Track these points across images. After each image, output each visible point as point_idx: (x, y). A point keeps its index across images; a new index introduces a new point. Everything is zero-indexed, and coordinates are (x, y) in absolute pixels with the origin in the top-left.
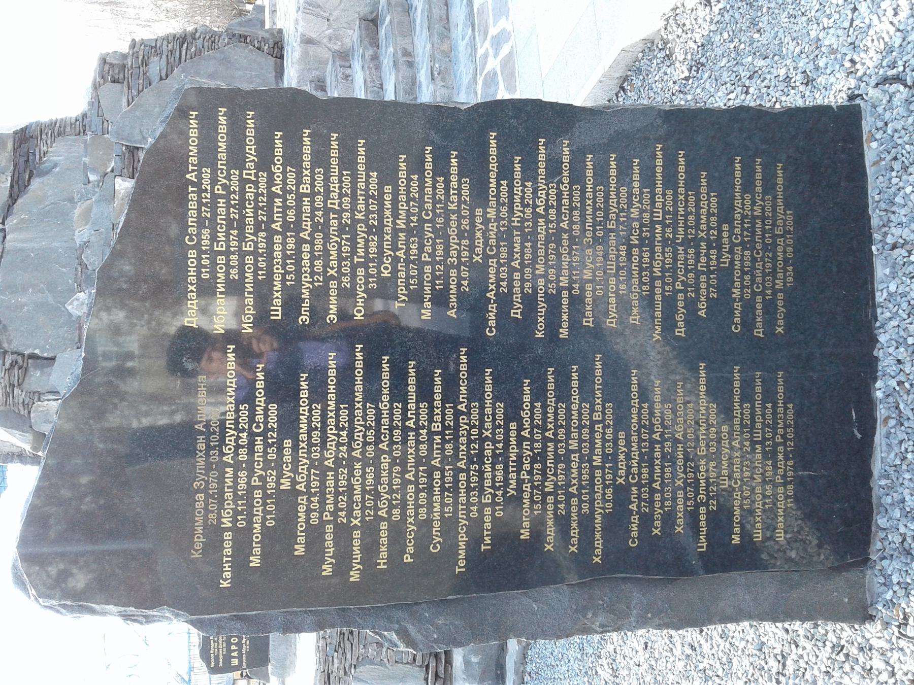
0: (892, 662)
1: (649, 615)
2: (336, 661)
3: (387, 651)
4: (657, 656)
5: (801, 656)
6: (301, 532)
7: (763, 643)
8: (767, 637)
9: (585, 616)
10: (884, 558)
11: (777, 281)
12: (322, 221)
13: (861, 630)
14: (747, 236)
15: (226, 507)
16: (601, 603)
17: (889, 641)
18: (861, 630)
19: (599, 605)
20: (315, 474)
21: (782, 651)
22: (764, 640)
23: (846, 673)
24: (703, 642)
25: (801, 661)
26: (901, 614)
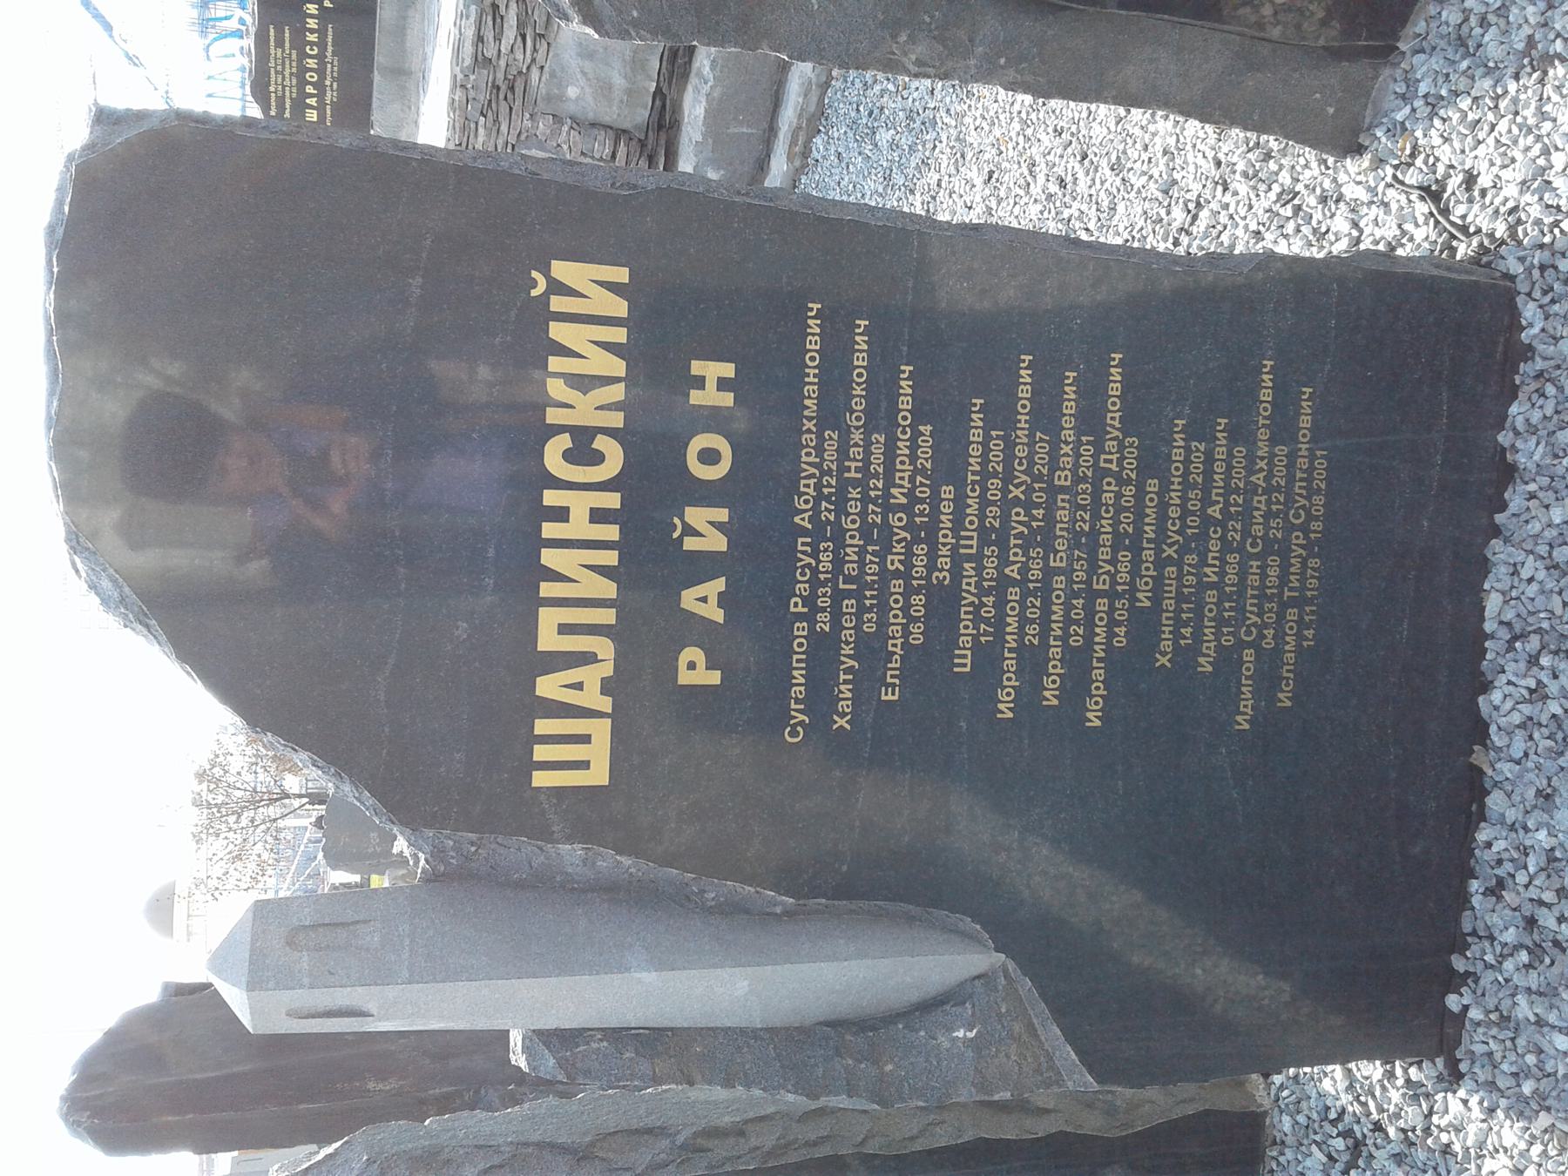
0: (1362, 224)
1: (1002, 61)
2: (481, 131)
3: (569, 133)
4: (1002, 194)
5: (1226, 207)
7: (1175, 182)
8: (1184, 173)
9: (894, 37)
10: (1422, 51)
12: (1130, 530)
13: (1335, 168)
14: (986, 633)
16: (928, 20)
17: (1372, 190)
18: (1335, 168)
19: (924, 22)
21: (1199, 196)
22: (1177, 176)
23: (1286, 236)
24: (1081, 175)
25: (1223, 213)
26: (1408, 146)
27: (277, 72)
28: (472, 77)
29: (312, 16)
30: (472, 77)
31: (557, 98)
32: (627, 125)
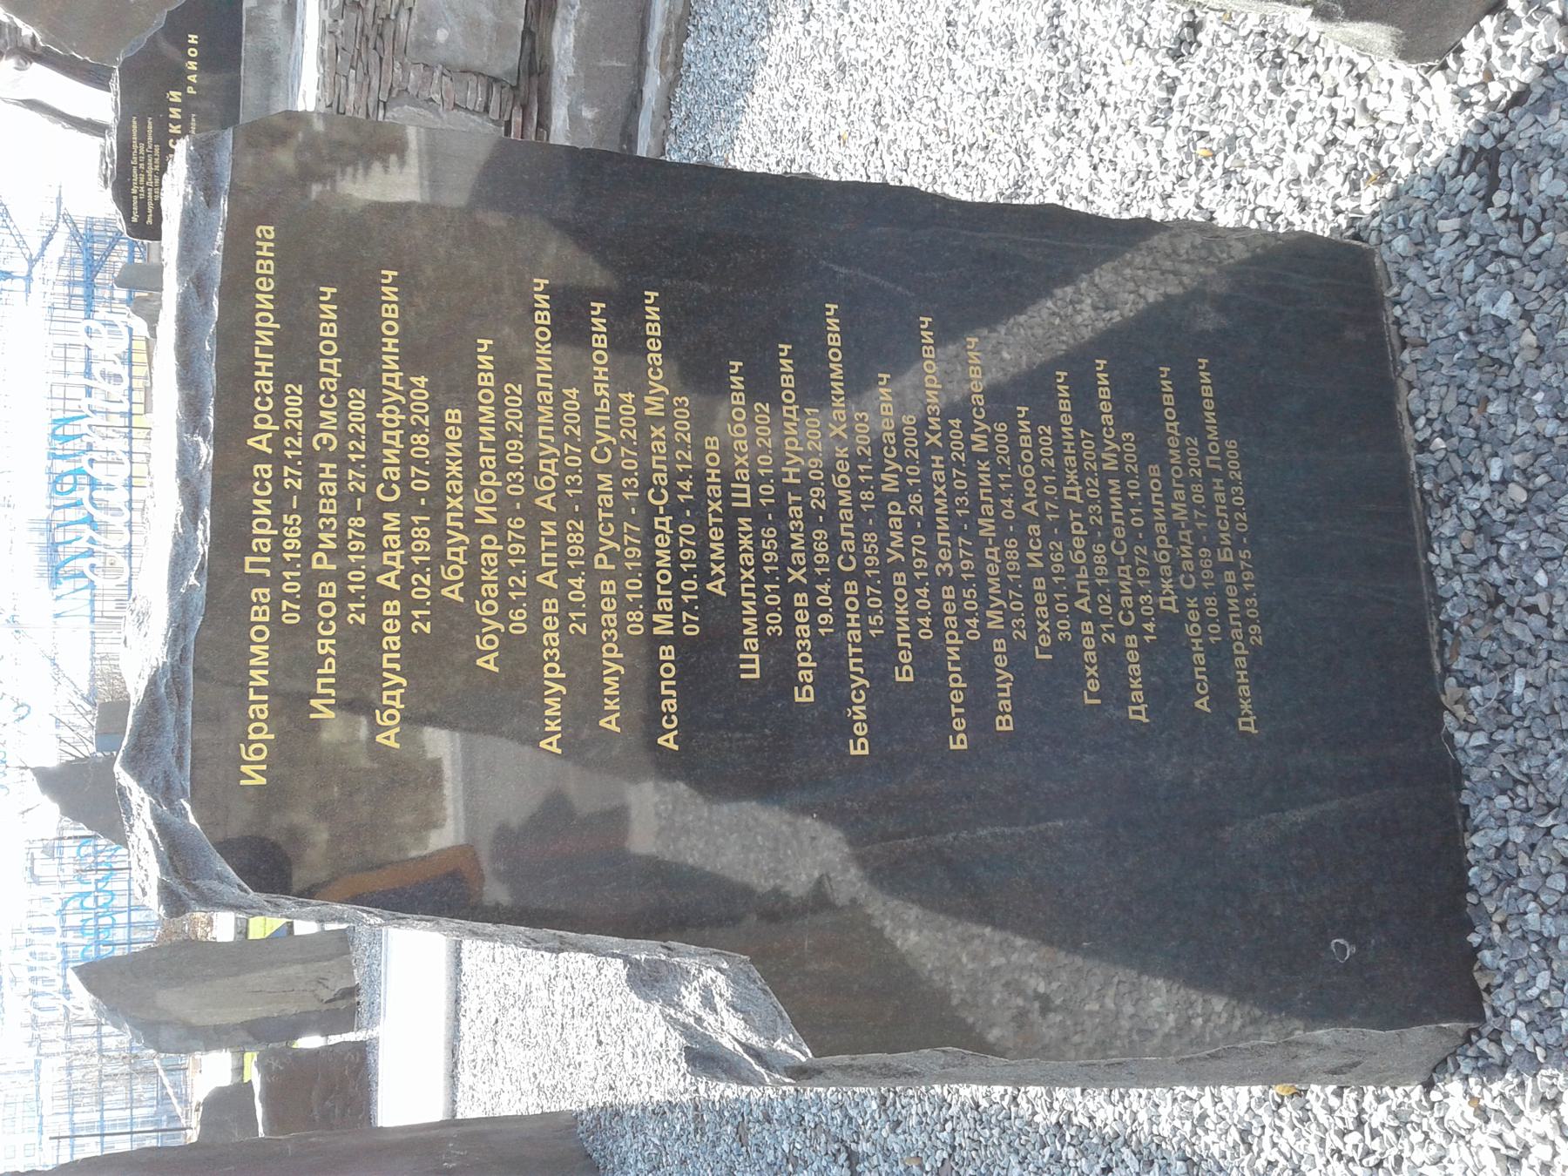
2: (352, 85)
6: (664, 587)
11: (1174, 506)
15: (252, 736)
20: (965, 547)
27: (139, 171)
28: (341, 22)
29: (175, 105)
30: (341, 22)
31: (425, 45)
32: (497, 71)
